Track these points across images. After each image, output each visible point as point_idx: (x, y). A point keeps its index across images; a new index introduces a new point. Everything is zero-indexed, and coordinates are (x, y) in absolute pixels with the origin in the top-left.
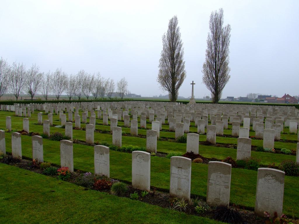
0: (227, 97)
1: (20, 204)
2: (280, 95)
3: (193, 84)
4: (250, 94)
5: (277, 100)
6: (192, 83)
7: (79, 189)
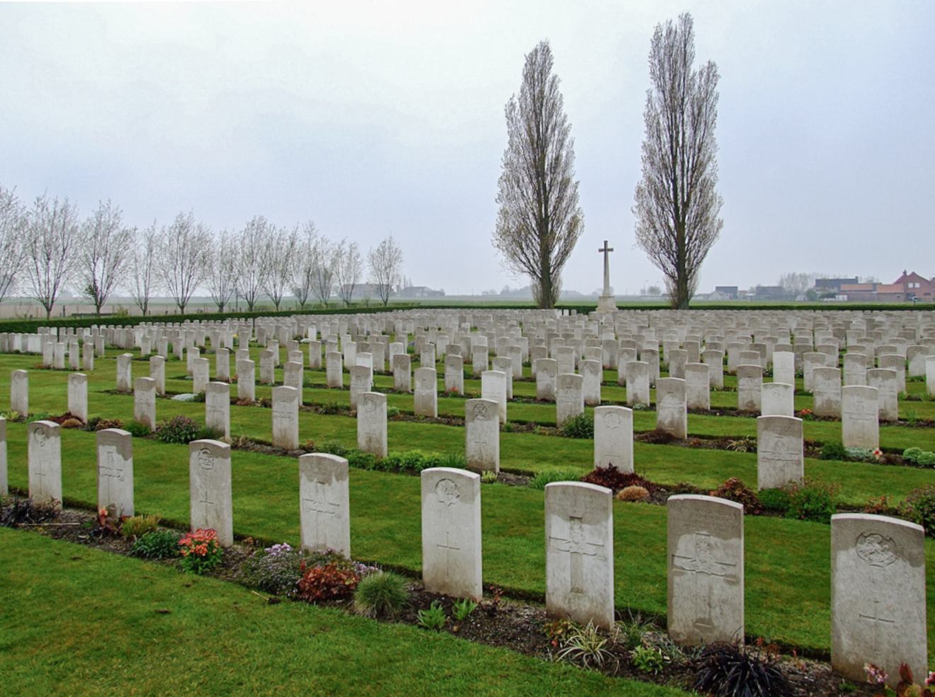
0: (714, 289)
3: (606, 250)
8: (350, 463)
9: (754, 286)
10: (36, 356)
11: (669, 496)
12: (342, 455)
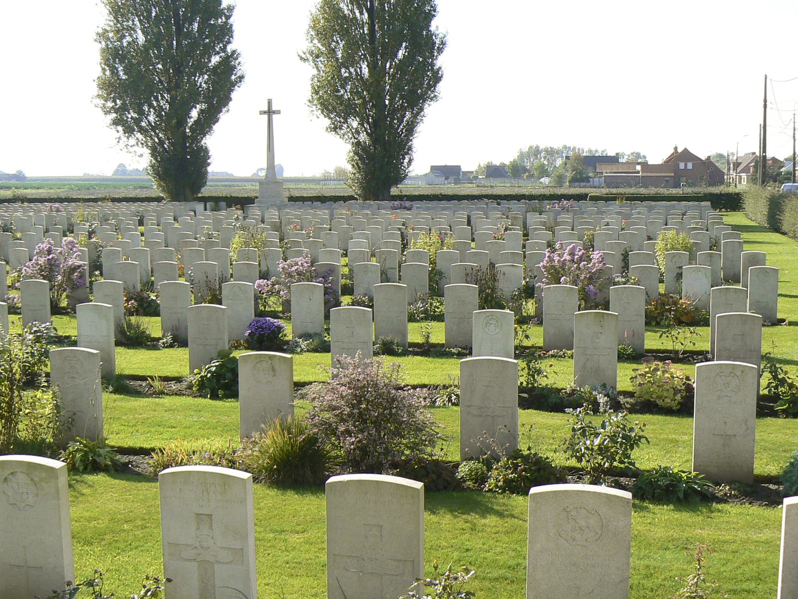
0: (428, 170)
1: (279, 578)
2: (657, 156)
3: (270, 112)
4: (531, 148)
5: (607, 171)
6: (266, 109)
7: (463, 529)
8: (73, 469)
9: (484, 163)
10: (780, 245)
11: (329, 477)
12: (54, 456)
